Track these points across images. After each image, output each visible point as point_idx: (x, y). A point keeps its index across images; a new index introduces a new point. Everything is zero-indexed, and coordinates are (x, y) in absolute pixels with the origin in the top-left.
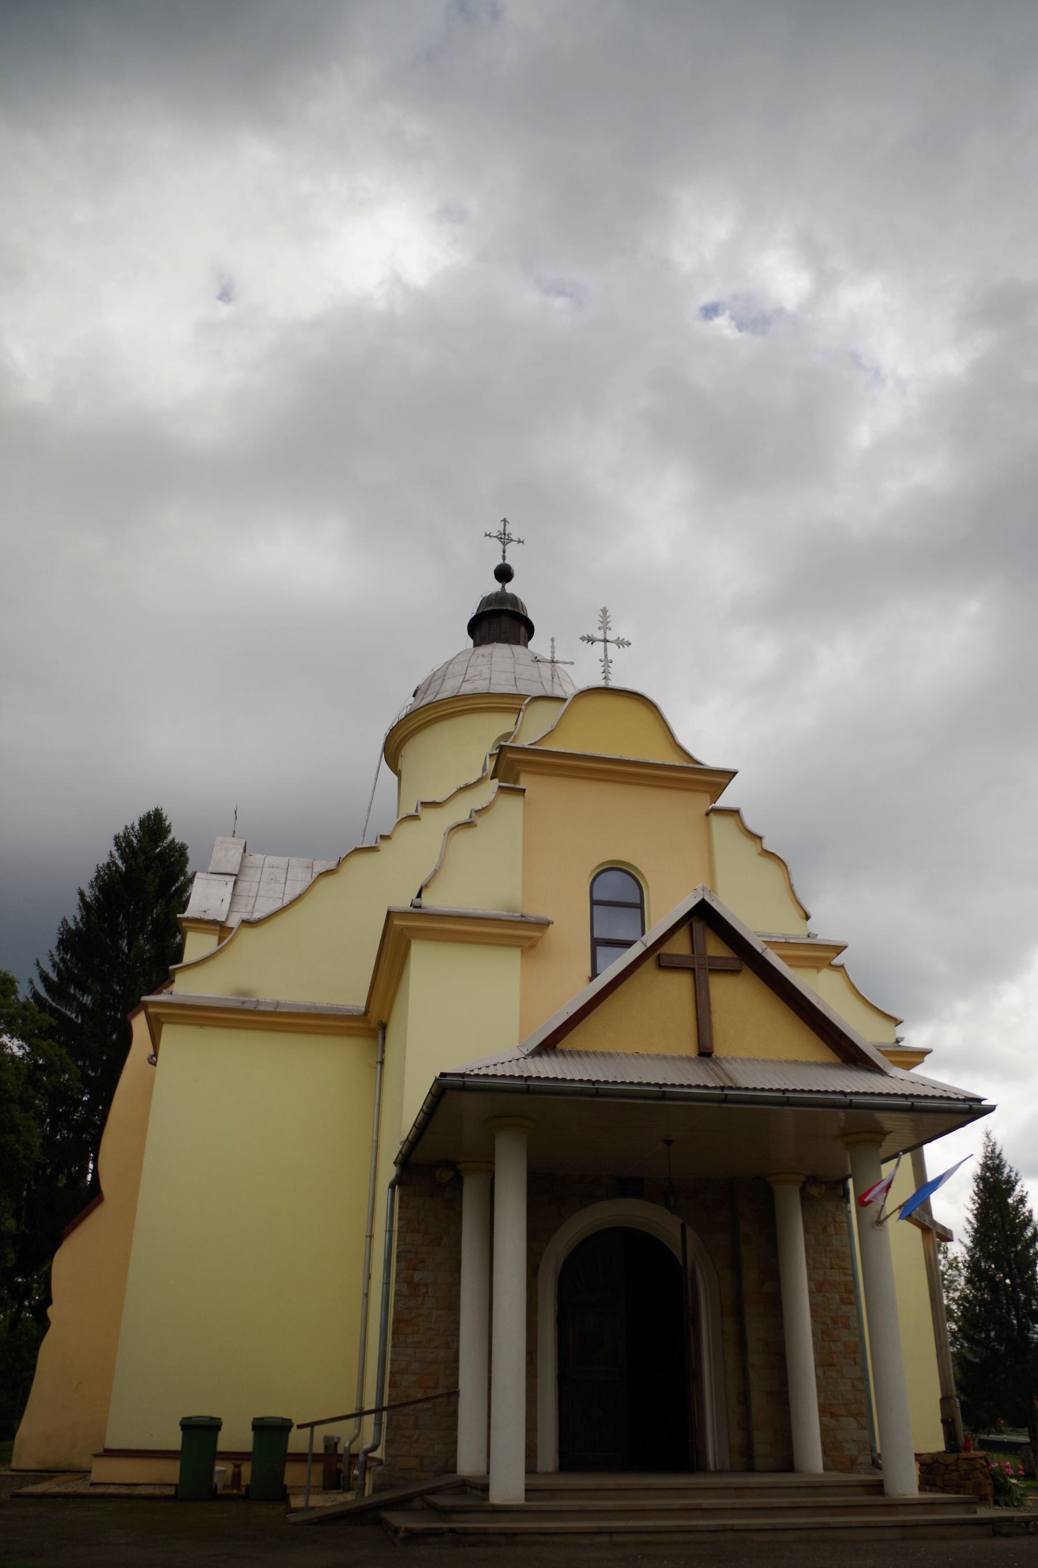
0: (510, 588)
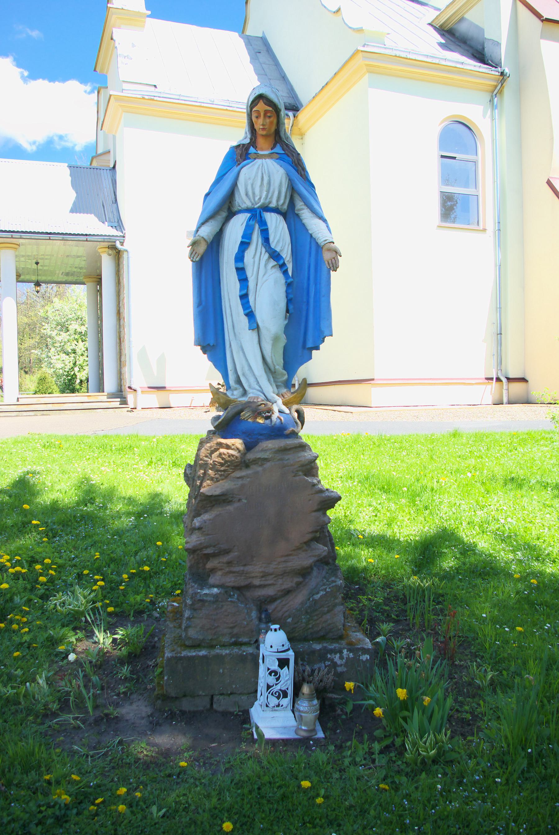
0: (39, 267)
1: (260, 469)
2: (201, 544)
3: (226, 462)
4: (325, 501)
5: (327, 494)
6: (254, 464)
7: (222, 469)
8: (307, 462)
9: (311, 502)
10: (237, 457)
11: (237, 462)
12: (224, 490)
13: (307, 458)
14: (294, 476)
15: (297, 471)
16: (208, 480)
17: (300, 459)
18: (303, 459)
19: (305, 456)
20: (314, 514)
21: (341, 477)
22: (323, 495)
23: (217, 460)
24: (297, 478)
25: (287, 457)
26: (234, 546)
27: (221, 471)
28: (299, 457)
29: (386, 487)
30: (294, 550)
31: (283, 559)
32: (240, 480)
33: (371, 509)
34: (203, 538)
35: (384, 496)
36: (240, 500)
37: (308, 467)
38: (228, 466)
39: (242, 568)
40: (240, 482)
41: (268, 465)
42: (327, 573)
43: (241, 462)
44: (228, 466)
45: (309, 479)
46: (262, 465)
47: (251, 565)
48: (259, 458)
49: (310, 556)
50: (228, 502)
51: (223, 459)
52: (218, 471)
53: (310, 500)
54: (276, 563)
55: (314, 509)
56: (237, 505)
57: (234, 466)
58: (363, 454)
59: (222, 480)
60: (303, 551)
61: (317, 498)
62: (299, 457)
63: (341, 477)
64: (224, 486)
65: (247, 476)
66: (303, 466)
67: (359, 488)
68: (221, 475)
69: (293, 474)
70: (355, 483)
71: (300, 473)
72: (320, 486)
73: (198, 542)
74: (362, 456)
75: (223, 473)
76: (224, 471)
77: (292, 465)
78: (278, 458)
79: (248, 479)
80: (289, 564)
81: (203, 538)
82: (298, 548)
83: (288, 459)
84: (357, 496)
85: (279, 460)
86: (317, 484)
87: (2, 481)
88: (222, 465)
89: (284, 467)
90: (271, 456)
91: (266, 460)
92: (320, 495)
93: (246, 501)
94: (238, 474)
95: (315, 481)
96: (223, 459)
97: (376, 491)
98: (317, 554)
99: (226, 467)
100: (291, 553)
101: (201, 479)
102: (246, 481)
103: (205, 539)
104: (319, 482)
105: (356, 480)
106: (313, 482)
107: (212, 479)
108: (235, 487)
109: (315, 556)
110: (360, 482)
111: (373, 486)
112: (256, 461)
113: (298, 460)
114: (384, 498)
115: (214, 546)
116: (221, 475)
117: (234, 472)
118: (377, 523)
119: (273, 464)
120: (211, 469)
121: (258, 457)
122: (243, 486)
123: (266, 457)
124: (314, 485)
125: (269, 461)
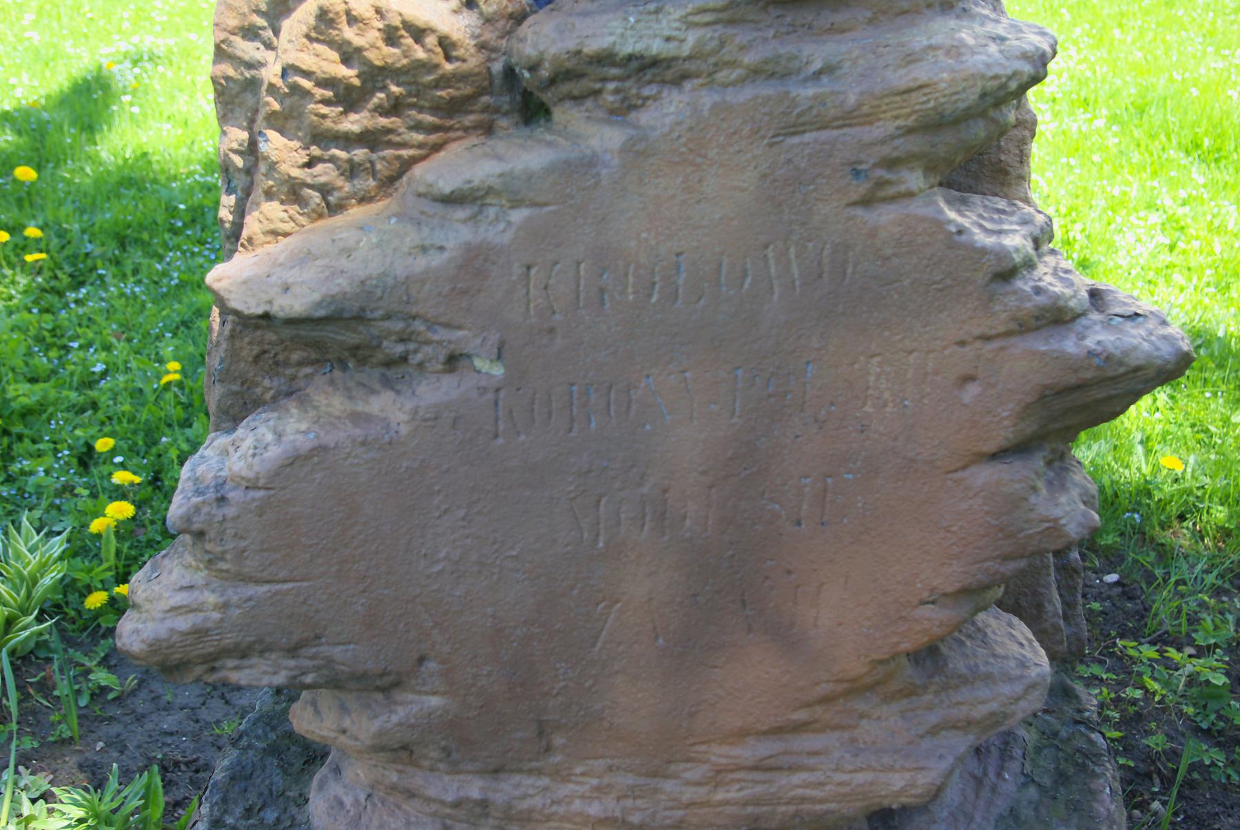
1: (605, 139)
2: (199, 633)
3: (375, 76)
4: (1081, 386)
5: (1098, 337)
6: (578, 99)
7: (353, 123)
8: (972, 97)
9: (973, 390)
10: (446, 45)
11: (445, 81)
12: (342, 284)
13: (975, 62)
14: (866, 202)
15: (891, 163)
16: (269, 195)
17: (921, 73)
18: (937, 73)
19: (956, 50)
20: (984, 475)
21: (1054, 101)
22: (1070, 346)
23: (306, 60)
24: (885, 216)
25: (816, 53)
26: (421, 660)
27: (347, 140)
28: (911, 59)
29: (1206, 143)
30: (826, 700)
31: (747, 752)
32: (461, 213)
33: (1155, 218)
34: (211, 598)
35: (1198, 175)
36: (453, 361)
37: (979, 130)
38: (395, 108)
39: (474, 789)
40: (457, 233)
41: (668, 111)
42: (1029, 780)
43: (483, 84)
44: (395, 108)
45: (972, 222)
46: (624, 110)
47: (539, 772)
48: (605, 59)
49: (934, 731)
50: (389, 363)
51: (349, 55)
52: (321, 137)
53: (968, 379)
54: (695, 773)
55: (991, 447)
56: (434, 391)
57: (435, 109)
58: (1120, 25)
59: (364, 200)
60: (889, 698)
61: (1028, 363)
62: (911, 59)
63: (1054, 101)
64: (348, 252)
65: (512, 192)
66: (935, 124)
67: (1112, 141)
68: (352, 171)
69: (860, 188)
70: (1100, 123)
71: (914, 179)
72: (1044, 275)
73: (183, 623)
74: (1117, 33)
75: (360, 154)
76: (370, 139)
77: (849, 118)
78: (749, 59)
79: (518, 216)
80: (793, 783)
81: (211, 598)
82: (856, 689)
83: (828, 70)
84: (1107, 168)
85: (755, 73)
86: (1029, 265)
87: (28, 85)
88: (348, 98)
89: (795, 129)
90: (692, 38)
91: (646, 67)
92: (1041, 344)
93: (498, 371)
94: (459, 164)
95: (1016, 241)
96: (349, 55)
97: (1172, 154)
98: (979, 712)
99: (381, 111)
100: (802, 715)
101: (240, 181)
102: (502, 228)
103: (225, 606)
104: (1041, 238)
105: (1104, 112)
106: (1001, 254)
107: (293, 193)
108: (420, 264)
109: (967, 725)
110: (1114, 119)
111: (1162, 137)
112: (581, 76)
113: (900, 78)
114: (1201, 180)
115: (293, 651)
116: (352, 171)
117: (437, 148)
118: (1178, 278)
119: (707, 100)
120: (280, 122)
121: (593, 46)
122: (475, 262)
123: (656, 47)
124: (1007, 272)
125: (679, 80)
